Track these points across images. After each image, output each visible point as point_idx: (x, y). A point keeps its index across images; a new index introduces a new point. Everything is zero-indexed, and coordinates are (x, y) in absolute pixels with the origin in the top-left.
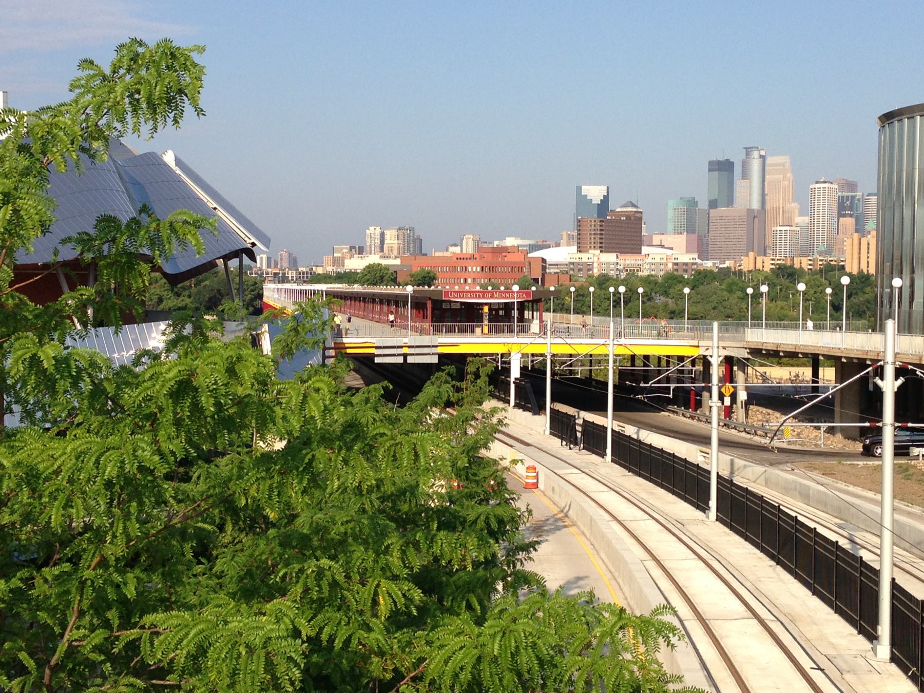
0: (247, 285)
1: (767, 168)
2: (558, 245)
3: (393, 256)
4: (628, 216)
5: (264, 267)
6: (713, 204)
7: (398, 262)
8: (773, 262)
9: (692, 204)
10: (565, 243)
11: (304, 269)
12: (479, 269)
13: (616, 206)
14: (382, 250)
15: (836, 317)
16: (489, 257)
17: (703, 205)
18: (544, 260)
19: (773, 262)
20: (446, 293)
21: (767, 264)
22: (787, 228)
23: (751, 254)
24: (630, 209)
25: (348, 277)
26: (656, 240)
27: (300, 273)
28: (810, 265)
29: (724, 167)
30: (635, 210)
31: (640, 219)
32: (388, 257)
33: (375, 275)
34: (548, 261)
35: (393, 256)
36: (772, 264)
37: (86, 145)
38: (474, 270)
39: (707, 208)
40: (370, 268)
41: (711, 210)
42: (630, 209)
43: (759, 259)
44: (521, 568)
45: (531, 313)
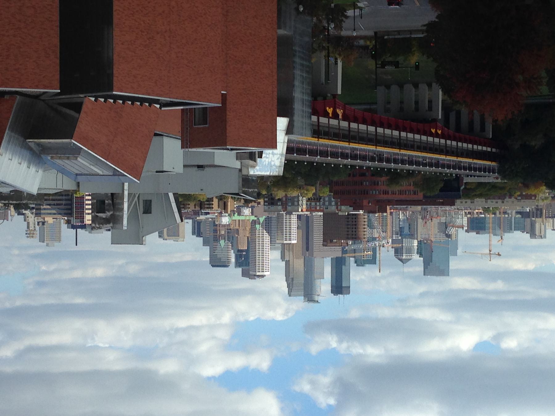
22: (285, 242)
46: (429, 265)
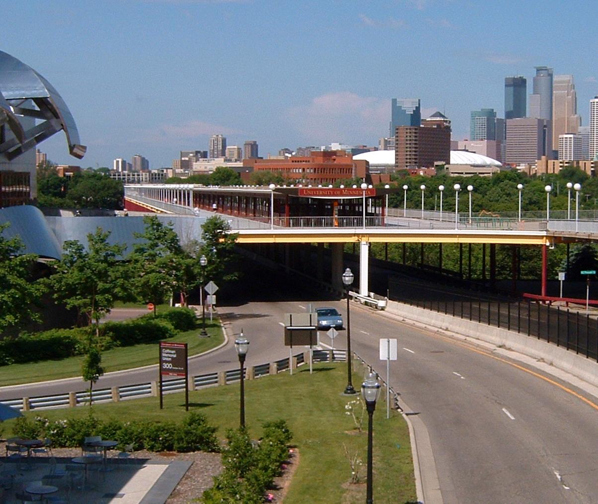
0: (93, 187)
1: (554, 85)
2: (376, 149)
3: (233, 159)
4: (439, 124)
5: (120, 170)
6: (509, 115)
7: (240, 164)
8: (561, 165)
9: (491, 114)
10: (383, 148)
11: (156, 172)
12: (312, 171)
13: (426, 115)
14: (223, 154)
15: (464, 209)
16: (320, 161)
17: (501, 115)
18: (367, 162)
19: (561, 165)
20: (302, 190)
21: (556, 167)
22: (572, 136)
23: (543, 157)
24: (438, 119)
25: (200, 178)
26: (461, 145)
27: (152, 174)
28: (592, 167)
29: (517, 85)
30: (443, 119)
31: (448, 129)
32: (230, 161)
33: (224, 176)
34: (370, 163)
35: (233, 159)
36: (561, 167)
37: (235, 498)
38: (297, 170)
39: (503, 117)
40: (219, 170)
41: (508, 120)
42: (438, 119)
43: (551, 162)
44: (208, 312)
45: (381, 209)
46: (414, 111)
